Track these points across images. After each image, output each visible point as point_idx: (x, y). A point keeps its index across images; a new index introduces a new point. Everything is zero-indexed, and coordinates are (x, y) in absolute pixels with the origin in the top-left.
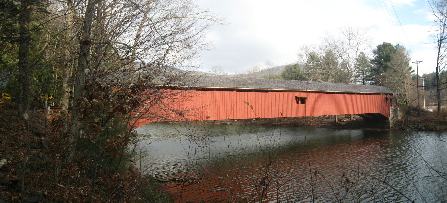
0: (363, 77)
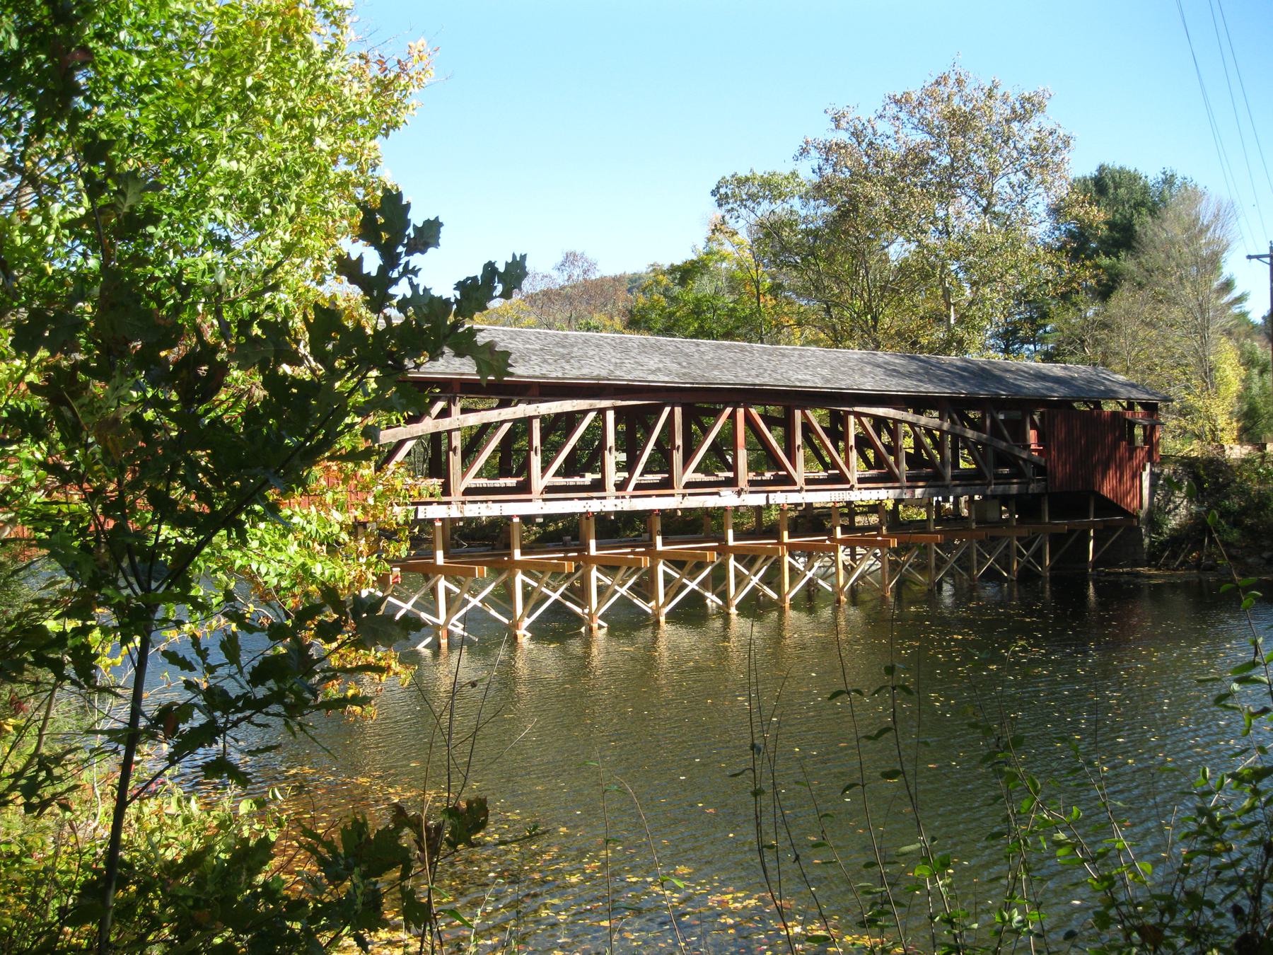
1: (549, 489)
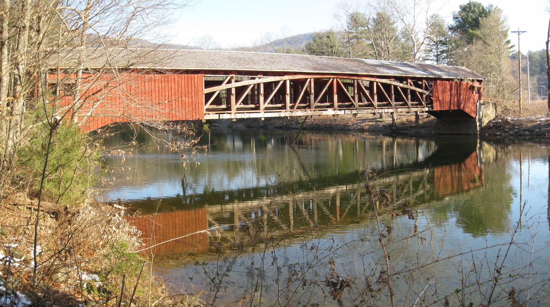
0: (437, 52)
1: (266, 109)
